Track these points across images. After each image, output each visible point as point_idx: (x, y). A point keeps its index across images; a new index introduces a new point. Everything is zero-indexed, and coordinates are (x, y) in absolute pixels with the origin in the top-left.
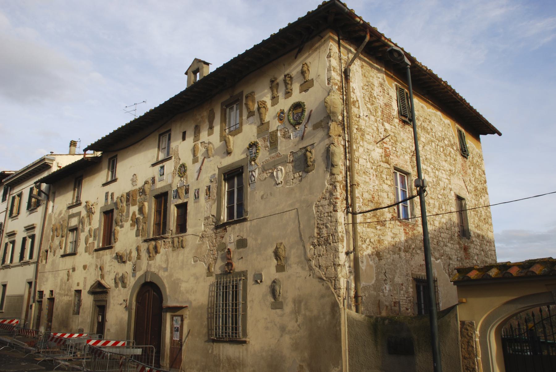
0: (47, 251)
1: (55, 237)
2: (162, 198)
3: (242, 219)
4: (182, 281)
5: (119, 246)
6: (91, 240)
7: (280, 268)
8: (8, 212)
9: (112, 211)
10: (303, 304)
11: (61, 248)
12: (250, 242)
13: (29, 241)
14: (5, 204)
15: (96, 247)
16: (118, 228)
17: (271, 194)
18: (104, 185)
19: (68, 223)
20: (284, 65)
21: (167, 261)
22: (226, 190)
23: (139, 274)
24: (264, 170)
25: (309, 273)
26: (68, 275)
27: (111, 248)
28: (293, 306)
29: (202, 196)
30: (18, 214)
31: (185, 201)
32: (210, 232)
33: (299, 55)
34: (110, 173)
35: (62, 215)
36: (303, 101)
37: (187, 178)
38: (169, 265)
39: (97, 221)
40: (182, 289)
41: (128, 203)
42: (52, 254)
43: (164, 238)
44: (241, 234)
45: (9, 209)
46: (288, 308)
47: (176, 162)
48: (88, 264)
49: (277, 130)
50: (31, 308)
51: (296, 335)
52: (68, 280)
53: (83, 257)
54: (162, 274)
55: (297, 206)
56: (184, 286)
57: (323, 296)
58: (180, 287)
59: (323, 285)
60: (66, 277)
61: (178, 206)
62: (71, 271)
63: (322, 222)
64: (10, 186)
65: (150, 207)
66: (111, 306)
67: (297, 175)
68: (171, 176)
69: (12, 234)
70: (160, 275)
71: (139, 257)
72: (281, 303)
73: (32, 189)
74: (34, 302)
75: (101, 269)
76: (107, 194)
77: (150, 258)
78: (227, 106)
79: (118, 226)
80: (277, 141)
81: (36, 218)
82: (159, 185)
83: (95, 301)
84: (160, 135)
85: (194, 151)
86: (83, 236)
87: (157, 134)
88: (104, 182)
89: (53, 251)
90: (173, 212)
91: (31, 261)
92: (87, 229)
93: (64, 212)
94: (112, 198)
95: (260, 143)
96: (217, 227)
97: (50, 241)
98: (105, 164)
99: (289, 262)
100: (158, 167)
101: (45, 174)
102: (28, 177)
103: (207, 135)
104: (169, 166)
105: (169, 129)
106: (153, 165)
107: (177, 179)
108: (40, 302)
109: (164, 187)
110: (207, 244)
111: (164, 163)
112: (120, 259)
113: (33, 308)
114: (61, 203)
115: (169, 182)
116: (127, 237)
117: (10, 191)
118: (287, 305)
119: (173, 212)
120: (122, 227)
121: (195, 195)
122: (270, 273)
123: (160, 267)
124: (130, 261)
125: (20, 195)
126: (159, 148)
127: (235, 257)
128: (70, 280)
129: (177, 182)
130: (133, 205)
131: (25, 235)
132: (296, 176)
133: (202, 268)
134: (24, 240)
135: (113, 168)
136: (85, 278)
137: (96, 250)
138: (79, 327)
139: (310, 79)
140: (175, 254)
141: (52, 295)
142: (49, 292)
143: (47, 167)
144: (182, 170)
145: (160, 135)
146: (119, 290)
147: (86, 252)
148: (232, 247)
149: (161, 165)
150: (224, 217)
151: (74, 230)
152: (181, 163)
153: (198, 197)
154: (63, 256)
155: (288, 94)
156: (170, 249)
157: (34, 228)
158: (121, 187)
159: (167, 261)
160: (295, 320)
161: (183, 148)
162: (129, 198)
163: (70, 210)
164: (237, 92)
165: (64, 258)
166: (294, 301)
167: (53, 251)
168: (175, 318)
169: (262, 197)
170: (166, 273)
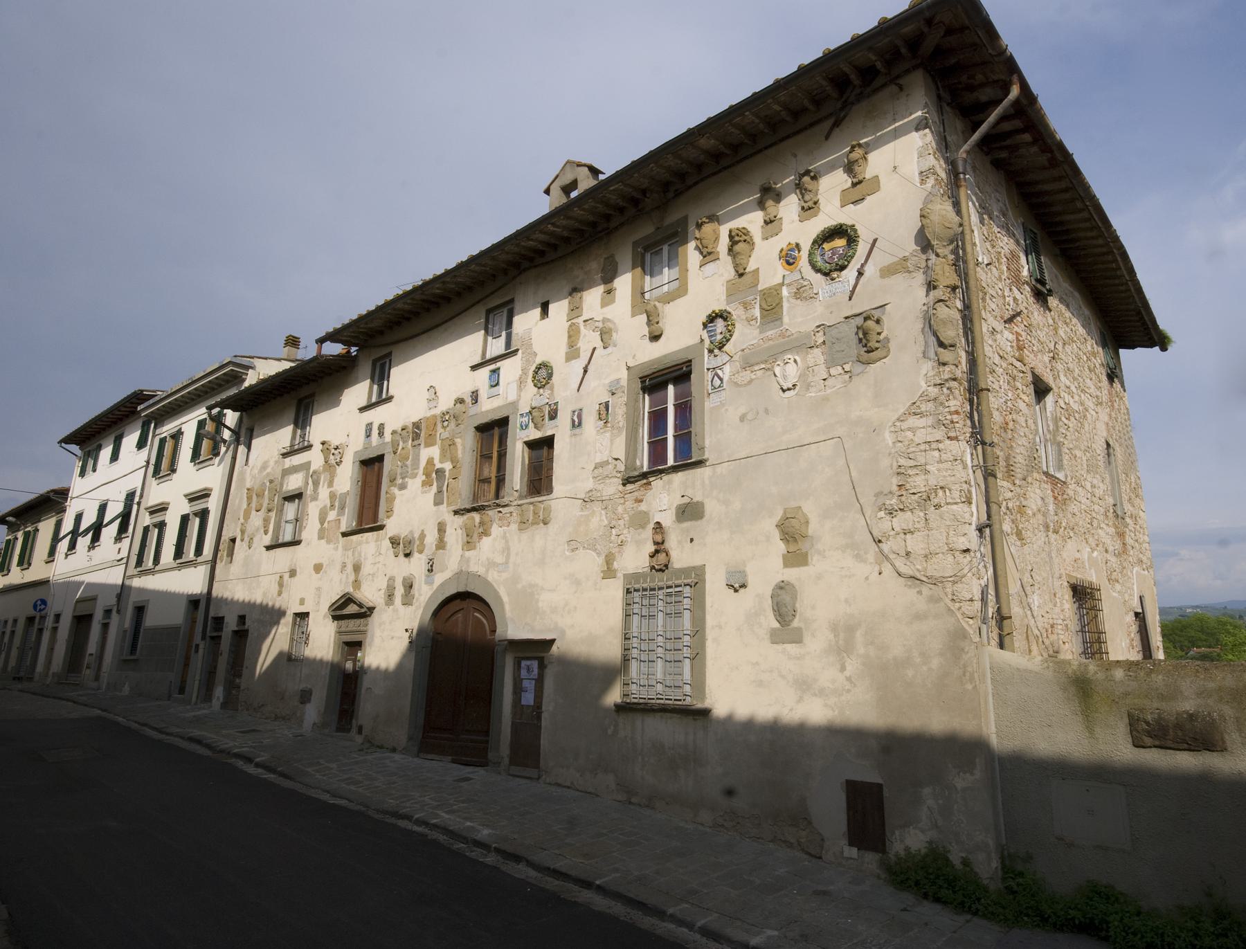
0: (233, 540)
1: (254, 512)
2: (494, 431)
3: (688, 461)
4: (542, 589)
5: (394, 525)
6: (332, 515)
7: (796, 558)
8: (151, 468)
9: (380, 459)
10: (859, 635)
11: (266, 533)
12: (711, 507)
13: (195, 523)
14: (144, 453)
15: (343, 529)
16: (395, 491)
17: (767, 411)
18: (362, 410)
19: (282, 485)
20: (795, 156)
21: (507, 550)
22: (647, 409)
23: (439, 578)
24: (747, 365)
25: (877, 569)
26: (281, 585)
27: (381, 528)
28: (831, 636)
29: (590, 422)
30: (174, 471)
31: (549, 433)
32: (613, 487)
33: (837, 130)
34: (375, 387)
35: (269, 470)
36: (850, 223)
37: (552, 389)
38: (512, 560)
39: (346, 478)
40: (540, 604)
41: (416, 442)
42: (245, 544)
43: (498, 505)
44: (689, 493)
45: (153, 461)
46: (817, 642)
47: (528, 361)
48: (325, 561)
49: (783, 284)
50: (197, 651)
51: (843, 698)
52: (280, 593)
53: (313, 548)
54: (492, 576)
55: (840, 431)
56: (545, 600)
57: (919, 617)
58: (537, 601)
59: (920, 593)
60: (275, 588)
61: (532, 445)
62: (286, 576)
63: (912, 463)
64: (155, 419)
65: (466, 444)
66: (377, 641)
67: (836, 370)
68: (514, 386)
69: (162, 508)
70: (490, 579)
71: (441, 544)
72: (799, 630)
73: (201, 424)
74: (203, 638)
75: (357, 568)
76: (369, 428)
77: (469, 544)
78: (646, 249)
79: (395, 486)
80: (780, 305)
81: (212, 476)
82: (489, 407)
83: (339, 633)
84: (489, 312)
85: (573, 335)
86: (313, 509)
87: (482, 310)
88: (364, 403)
89: (246, 539)
90: (518, 456)
91: (200, 559)
92: (324, 492)
93: (272, 463)
94: (381, 434)
95: (737, 312)
96: (627, 481)
97: (242, 520)
98: (365, 368)
99: (819, 546)
100: (485, 371)
101: (233, 391)
102: (199, 396)
103: (838, 203)
104: (510, 369)
105: (507, 299)
106: (474, 368)
107: (531, 389)
108: (216, 639)
109: (499, 408)
110: (599, 519)
111: (498, 364)
112: (404, 547)
113: (201, 651)
114: (271, 444)
115: (512, 397)
116: (411, 507)
117: (155, 428)
118: (813, 635)
119: (518, 456)
120: (403, 487)
121: (573, 421)
122: (767, 567)
123: (491, 564)
124: (421, 552)
125: (177, 436)
126: (487, 332)
127: (673, 543)
128: (284, 595)
129: (530, 397)
130: (428, 445)
131: (186, 508)
132: (833, 371)
133: (591, 562)
134: (185, 520)
135: (380, 375)
136: (318, 589)
137: (344, 535)
138: (303, 686)
139: (868, 176)
140: (525, 536)
141: (244, 624)
142: (236, 619)
143: (235, 378)
144: (543, 375)
145: (489, 312)
146: (396, 611)
147: (320, 537)
148: (667, 519)
149: (493, 367)
150: (644, 463)
151: (297, 496)
152: (538, 361)
153: (580, 424)
154: (268, 548)
155: (809, 209)
156: (514, 527)
157: (207, 495)
158: (392, 417)
159: (507, 550)
160: (839, 666)
161: (540, 329)
162: (416, 432)
163: (287, 460)
164: (672, 217)
165: (272, 552)
166: (834, 628)
167: (246, 539)
168: (524, 663)
169: (742, 419)
170: (505, 575)
